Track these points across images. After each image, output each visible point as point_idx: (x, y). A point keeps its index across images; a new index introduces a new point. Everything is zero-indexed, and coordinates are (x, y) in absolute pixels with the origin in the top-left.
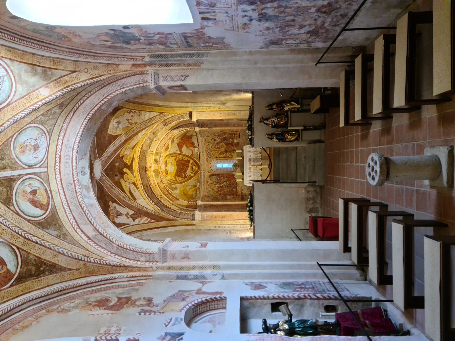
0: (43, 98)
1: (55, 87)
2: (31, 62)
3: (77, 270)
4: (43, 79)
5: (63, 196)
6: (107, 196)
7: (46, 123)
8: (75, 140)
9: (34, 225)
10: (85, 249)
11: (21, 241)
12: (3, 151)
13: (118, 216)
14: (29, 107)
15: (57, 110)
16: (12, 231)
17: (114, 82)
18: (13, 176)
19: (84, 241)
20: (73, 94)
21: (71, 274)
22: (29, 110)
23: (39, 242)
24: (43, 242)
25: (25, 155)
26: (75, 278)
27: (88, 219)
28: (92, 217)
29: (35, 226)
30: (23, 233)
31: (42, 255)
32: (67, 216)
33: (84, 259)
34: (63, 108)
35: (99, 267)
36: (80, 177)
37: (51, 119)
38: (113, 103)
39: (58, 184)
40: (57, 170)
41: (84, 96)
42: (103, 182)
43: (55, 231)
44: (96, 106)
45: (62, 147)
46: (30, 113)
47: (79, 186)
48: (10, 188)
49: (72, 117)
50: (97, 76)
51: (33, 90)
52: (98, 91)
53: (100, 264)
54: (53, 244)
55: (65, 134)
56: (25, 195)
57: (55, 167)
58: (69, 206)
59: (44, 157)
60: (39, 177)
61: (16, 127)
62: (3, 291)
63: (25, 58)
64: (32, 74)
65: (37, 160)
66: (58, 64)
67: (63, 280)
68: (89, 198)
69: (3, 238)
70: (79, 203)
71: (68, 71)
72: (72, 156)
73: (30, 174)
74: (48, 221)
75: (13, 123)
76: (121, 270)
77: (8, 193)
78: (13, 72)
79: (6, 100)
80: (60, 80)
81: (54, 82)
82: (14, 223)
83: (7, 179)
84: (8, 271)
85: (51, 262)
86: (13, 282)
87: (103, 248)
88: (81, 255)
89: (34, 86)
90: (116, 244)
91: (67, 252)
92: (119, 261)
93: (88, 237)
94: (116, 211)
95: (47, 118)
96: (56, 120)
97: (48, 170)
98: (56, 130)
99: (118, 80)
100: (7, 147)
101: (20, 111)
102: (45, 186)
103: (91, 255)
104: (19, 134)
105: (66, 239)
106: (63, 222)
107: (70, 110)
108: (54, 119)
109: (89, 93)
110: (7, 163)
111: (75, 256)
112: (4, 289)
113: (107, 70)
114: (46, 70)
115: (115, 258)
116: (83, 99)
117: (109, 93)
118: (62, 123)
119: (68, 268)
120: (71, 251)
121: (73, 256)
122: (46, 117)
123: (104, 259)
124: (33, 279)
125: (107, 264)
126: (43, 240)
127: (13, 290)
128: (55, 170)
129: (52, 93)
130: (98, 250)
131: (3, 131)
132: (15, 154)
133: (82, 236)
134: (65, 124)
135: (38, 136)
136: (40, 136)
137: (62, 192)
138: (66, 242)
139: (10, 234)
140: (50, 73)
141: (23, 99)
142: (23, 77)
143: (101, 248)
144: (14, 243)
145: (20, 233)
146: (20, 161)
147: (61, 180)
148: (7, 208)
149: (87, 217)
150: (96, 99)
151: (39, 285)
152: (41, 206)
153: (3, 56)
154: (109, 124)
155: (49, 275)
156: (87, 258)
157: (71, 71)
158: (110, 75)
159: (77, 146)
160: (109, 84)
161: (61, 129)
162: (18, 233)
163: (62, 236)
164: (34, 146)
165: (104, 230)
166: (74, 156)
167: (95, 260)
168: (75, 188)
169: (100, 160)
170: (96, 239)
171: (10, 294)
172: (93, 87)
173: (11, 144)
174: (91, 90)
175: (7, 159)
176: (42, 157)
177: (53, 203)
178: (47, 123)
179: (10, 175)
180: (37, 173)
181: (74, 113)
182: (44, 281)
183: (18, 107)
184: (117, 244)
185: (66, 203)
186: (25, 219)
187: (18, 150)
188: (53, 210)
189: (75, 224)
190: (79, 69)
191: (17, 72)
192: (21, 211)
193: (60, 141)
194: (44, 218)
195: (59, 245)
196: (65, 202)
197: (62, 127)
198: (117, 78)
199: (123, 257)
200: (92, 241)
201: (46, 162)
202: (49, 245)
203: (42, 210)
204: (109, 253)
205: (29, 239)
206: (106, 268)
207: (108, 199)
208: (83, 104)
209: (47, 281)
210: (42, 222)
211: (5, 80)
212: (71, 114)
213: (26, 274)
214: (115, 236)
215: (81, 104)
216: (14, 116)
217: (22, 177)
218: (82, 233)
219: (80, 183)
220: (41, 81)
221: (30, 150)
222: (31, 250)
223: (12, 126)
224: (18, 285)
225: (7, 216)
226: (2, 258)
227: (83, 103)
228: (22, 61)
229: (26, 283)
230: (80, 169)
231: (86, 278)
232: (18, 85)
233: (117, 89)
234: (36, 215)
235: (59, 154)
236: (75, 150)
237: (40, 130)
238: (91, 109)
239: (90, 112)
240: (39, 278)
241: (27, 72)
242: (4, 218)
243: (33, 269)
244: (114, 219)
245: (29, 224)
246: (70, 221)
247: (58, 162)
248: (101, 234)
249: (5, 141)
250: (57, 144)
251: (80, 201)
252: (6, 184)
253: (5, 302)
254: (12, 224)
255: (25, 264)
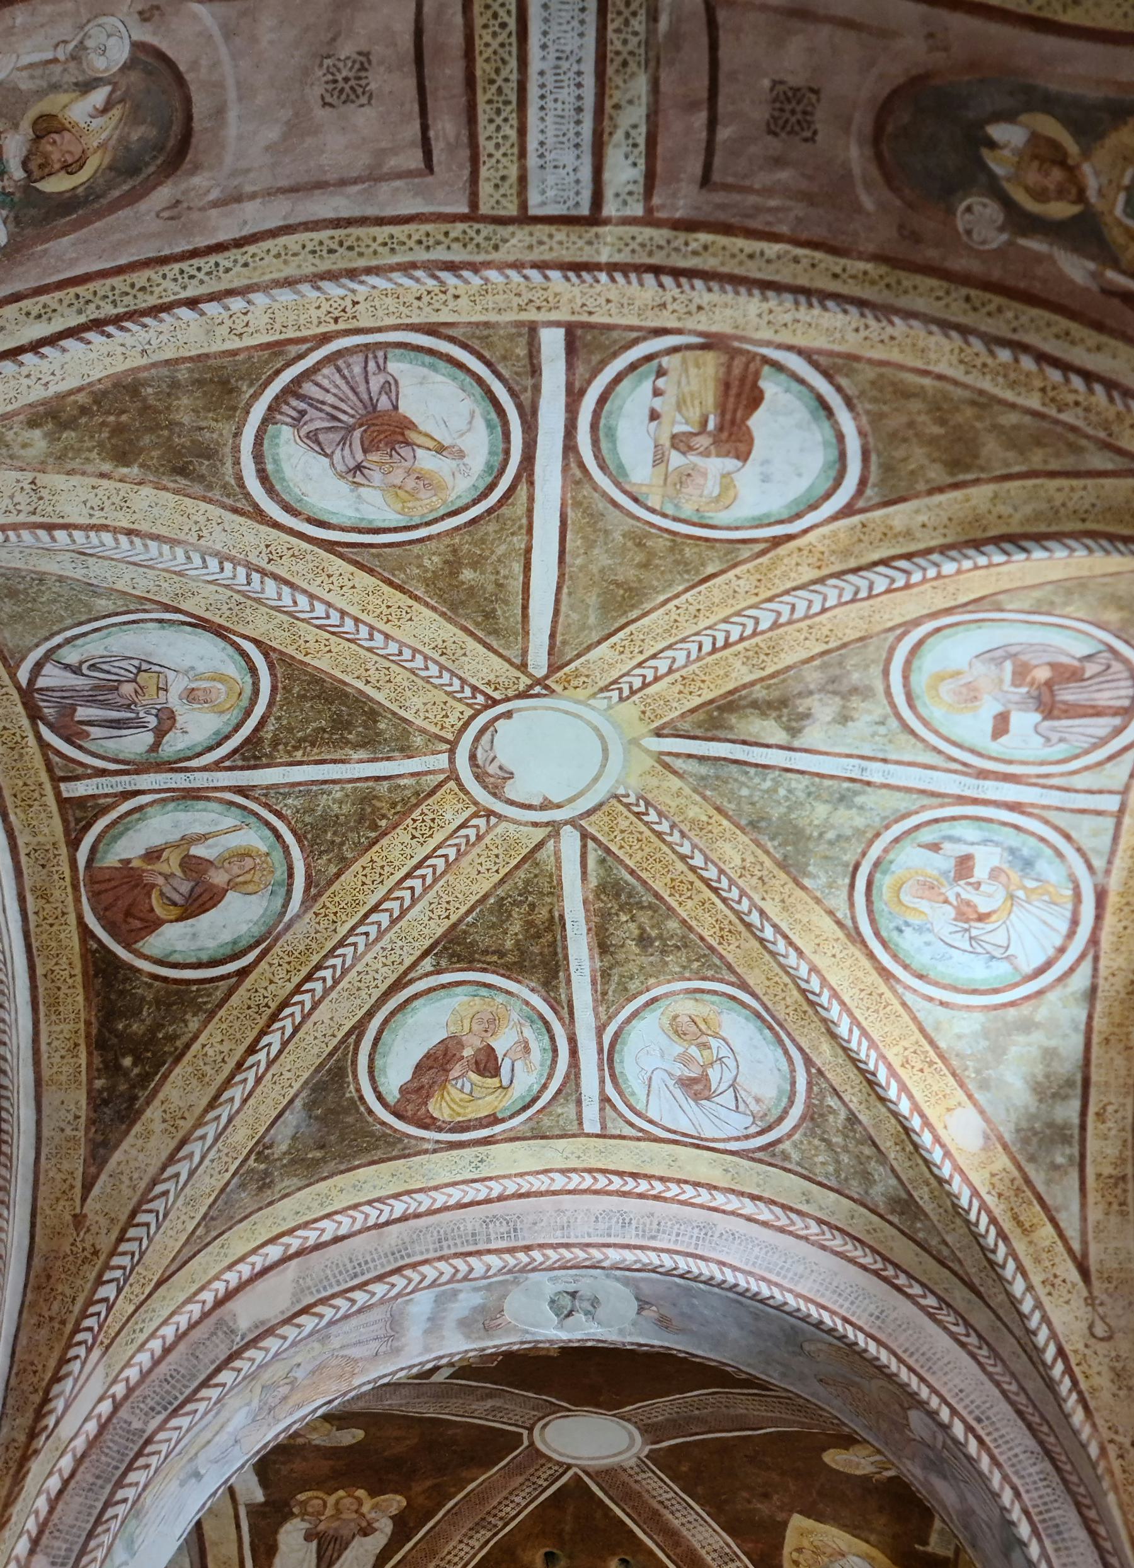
0: (933, 1120)
1: (993, 1175)
2: (1094, 1078)
3: (75, 1216)
4: (1024, 1124)
5: (456, 1195)
6: (435, 1487)
7: (813, 1134)
8: (734, 1269)
9: (336, 1049)
10: (173, 1268)
11: (272, 987)
12: (678, 948)
13: (314, 1545)
14: (883, 1057)
15: (883, 1187)
16: (326, 957)
17: (1065, 1482)
18: (569, 981)
19: (212, 1273)
20: (968, 1263)
21: (66, 1186)
22: (868, 1056)
23: (251, 1060)
24: (251, 1076)
25: (663, 1040)
26: (40, 1203)
27: (323, 1301)
28: (332, 1323)
29: (331, 1055)
30: (307, 997)
31: (190, 1069)
32: (355, 1207)
33: (124, 1254)
34: (895, 1219)
35: (63, 1323)
36: (548, 1285)
37: (838, 1162)
38: (945, 1478)
39: (519, 1180)
40: (588, 1181)
41: (967, 1324)
42: (517, 1469)
43: (294, 1138)
44: (922, 1379)
45: (702, 1206)
46: (855, 1061)
47: (500, 1272)
48: (515, 968)
49: (852, 1261)
50: (1083, 1385)
51: (967, 1081)
52: (1004, 1393)
53: (77, 1330)
54: (230, 1121)
55: (765, 1224)
56: (481, 1023)
57: (603, 1171)
58: (404, 1218)
59: (651, 1122)
60: (559, 1092)
61: (789, 1001)
62: (70, 900)
63: (1113, 1053)
64: (1040, 1078)
65: (641, 1093)
66: (1111, 1199)
67: (44, 1151)
68: (434, 1324)
69: (298, 916)
70: (414, 1266)
71: (1084, 1243)
72: (654, 1249)
73: (574, 1052)
74: (346, 1111)
75: (803, 992)
76: (15, 1434)
77: (494, 953)
78: (1033, 1001)
79: (906, 967)
80: (1030, 1203)
81: (1016, 1173)
82: (359, 967)
83: (556, 954)
84: (153, 924)
85: (148, 1103)
86: (99, 941)
87: (156, 1363)
88: (145, 1242)
89: (984, 1085)
90: (161, 1428)
91: (177, 1175)
92: (66, 1430)
93: (230, 1295)
94: (345, 1532)
95: (837, 1140)
96: (833, 1183)
97: (588, 1135)
98: (788, 1186)
99: (1078, 1506)
100: (695, 965)
101: (861, 1019)
102: (512, 1117)
103: (136, 1291)
104: (759, 1016)
105: (242, 1186)
106: (330, 1182)
107: (888, 1255)
108: (837, 1172)
109: (985, 1352)
110: (627, 960)
111: (150, 1211)
112: (77, 901)
113: (1119, 1439)
114: (1070, 1144)
115: (86, 1420)
116: (951, 1319)
117: (996, 1452)
118: (819, 1215)
119: (96, 1177)
120: (177, 1197)
121: (152, 1200)
122: (846, 1136)
123: (96, 1353)
124: (88, 1023)
125: (64, 1361)
126: (258, 1080)
127: (62, 936)
128: (590, 1171)
129: (961, 1162)
130: (153, 1335)
131: (765, 948)
132: (666, 995)
133: (239, 1267)
134: (814, 1228)
135: (750, 1100)
136: (754, 1107)
137: (472, 1193)
138: (228, 1184)
139: (314, 946)
140: (1060, 1160)
141: (918, 1035)
142: (1021, 1039)
143: (158, 1352)
144: (268, 958)
145: (307, 986)
146: (635, 1014)
147: (540, 1194)
148: (427, 943)
149: (334, 1296)
150: (957, 1381)
151: (55, 1043)
152: (422, 1087)
153: (1102, 963)
154: (844, 1527)
155: (89, 1092)
156: (124, 1268)
157: (1085, 1254)
158: (1094, 1450)
159: (707, 1273)
160: (1048, 1453)
161: (791, 1209)
162: (309, 978)
163: (263, 1166)
164: (705, 1079)
165: (251, 1377)
166: (652, 1255)
167: (102, 1308)
168: (489, 1252)
169: (641, 1464)
170: (213, 1334)
171: (51, 925)
172: (1021, 1364)
173: (712, 979)
174: (1005, 1356)
175: (643, 960)
176: (651, 1114)
177: (426, 1146)
178: (816, 1142)
179: (572, 969)
180: (578, 1085)
181: (876, 1273)
182: (64, 1069)
183: (877, 1011)
184: (161, 1436)
185: (422, 1209)
186: (370, 1014)
187: (686, 1007)
188: (392, 1145)
189: (311, 1243)
190: (1104, 1297)
191: (1038, 1018)
192: (408, 1001)
193: (734, 1203)
194: (361, 1098)
195: (219, 1144)
196: (425, 1202)
197: (799, 1213)
198: (1087, 1501)
199: (79, 1461)
200: (205, 1315)
201: (628, 1131)
202: (232, 1099)
203: (403, 1090)
204: (119, 1390)
205: (274, 1018)
206: (48, 1358)
207: (417, 1488)
208: (926, 1319)
209: (63, 1078)
210: (342, 1087)
211: (994, 963)
212: (867, 1260)
213: (122, 993)
214: (207, 1435)
215: (923, 1308)
216: (835, 995)
217: (560, 1019)
218: (258, 1268)
219: (516, 1282)
220: (1013, 1117)
221: (685, 1060)
222: (224, 1026)
223: (791, 986)
224: (83, 957)
225: (392, 941)
226: (215, 906)
227: (932, 1316)
228: (1096, 1039)
229: (80, 990)
230: (586, 1283)
231: (25, 1261)
232: (979, 1016)
233: (1025, 1496)
234: (379, 1063)
235: (668, 1195)
236: (683, 1264)
237: (780, 1109)
238: (899, 1352)
239: (886, 1347)
240: (88, 1046)
241: (1044, 1058)
242: (388, 929)
243: (135, 1027)
244: (303, 1514)
245: (346, 1029)
246: (328, 1216)
247: (626, 1188)
248: (231, 1358)
249: (721, 957)
250: (715, 1188)
251: (424, 1269)
252: (536, 950)
253: (22, 899)
254: (356, 958)
255: (168, 993)
